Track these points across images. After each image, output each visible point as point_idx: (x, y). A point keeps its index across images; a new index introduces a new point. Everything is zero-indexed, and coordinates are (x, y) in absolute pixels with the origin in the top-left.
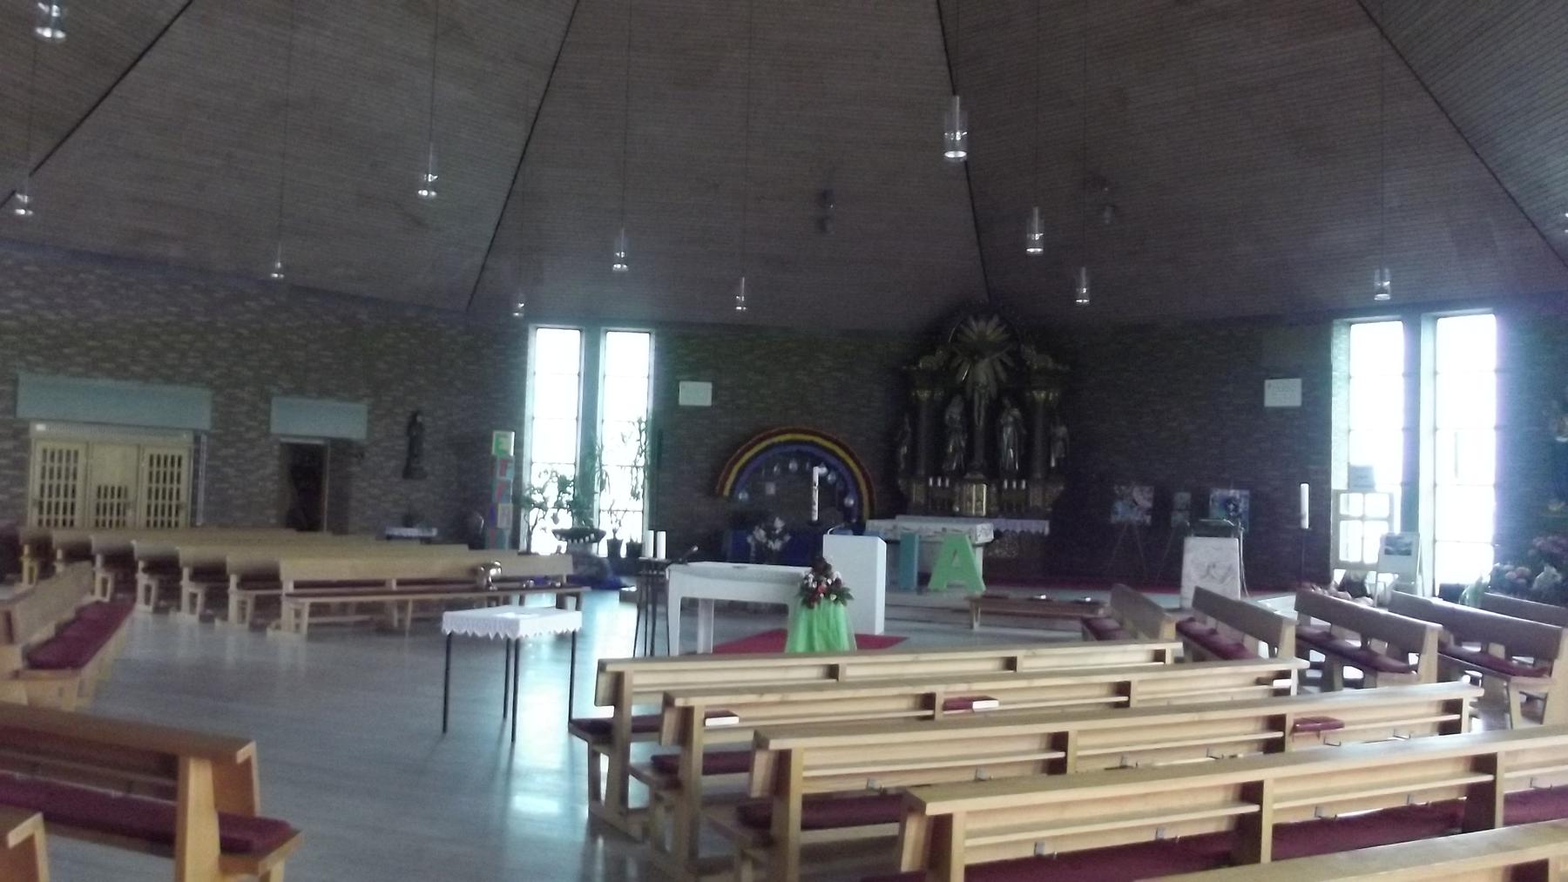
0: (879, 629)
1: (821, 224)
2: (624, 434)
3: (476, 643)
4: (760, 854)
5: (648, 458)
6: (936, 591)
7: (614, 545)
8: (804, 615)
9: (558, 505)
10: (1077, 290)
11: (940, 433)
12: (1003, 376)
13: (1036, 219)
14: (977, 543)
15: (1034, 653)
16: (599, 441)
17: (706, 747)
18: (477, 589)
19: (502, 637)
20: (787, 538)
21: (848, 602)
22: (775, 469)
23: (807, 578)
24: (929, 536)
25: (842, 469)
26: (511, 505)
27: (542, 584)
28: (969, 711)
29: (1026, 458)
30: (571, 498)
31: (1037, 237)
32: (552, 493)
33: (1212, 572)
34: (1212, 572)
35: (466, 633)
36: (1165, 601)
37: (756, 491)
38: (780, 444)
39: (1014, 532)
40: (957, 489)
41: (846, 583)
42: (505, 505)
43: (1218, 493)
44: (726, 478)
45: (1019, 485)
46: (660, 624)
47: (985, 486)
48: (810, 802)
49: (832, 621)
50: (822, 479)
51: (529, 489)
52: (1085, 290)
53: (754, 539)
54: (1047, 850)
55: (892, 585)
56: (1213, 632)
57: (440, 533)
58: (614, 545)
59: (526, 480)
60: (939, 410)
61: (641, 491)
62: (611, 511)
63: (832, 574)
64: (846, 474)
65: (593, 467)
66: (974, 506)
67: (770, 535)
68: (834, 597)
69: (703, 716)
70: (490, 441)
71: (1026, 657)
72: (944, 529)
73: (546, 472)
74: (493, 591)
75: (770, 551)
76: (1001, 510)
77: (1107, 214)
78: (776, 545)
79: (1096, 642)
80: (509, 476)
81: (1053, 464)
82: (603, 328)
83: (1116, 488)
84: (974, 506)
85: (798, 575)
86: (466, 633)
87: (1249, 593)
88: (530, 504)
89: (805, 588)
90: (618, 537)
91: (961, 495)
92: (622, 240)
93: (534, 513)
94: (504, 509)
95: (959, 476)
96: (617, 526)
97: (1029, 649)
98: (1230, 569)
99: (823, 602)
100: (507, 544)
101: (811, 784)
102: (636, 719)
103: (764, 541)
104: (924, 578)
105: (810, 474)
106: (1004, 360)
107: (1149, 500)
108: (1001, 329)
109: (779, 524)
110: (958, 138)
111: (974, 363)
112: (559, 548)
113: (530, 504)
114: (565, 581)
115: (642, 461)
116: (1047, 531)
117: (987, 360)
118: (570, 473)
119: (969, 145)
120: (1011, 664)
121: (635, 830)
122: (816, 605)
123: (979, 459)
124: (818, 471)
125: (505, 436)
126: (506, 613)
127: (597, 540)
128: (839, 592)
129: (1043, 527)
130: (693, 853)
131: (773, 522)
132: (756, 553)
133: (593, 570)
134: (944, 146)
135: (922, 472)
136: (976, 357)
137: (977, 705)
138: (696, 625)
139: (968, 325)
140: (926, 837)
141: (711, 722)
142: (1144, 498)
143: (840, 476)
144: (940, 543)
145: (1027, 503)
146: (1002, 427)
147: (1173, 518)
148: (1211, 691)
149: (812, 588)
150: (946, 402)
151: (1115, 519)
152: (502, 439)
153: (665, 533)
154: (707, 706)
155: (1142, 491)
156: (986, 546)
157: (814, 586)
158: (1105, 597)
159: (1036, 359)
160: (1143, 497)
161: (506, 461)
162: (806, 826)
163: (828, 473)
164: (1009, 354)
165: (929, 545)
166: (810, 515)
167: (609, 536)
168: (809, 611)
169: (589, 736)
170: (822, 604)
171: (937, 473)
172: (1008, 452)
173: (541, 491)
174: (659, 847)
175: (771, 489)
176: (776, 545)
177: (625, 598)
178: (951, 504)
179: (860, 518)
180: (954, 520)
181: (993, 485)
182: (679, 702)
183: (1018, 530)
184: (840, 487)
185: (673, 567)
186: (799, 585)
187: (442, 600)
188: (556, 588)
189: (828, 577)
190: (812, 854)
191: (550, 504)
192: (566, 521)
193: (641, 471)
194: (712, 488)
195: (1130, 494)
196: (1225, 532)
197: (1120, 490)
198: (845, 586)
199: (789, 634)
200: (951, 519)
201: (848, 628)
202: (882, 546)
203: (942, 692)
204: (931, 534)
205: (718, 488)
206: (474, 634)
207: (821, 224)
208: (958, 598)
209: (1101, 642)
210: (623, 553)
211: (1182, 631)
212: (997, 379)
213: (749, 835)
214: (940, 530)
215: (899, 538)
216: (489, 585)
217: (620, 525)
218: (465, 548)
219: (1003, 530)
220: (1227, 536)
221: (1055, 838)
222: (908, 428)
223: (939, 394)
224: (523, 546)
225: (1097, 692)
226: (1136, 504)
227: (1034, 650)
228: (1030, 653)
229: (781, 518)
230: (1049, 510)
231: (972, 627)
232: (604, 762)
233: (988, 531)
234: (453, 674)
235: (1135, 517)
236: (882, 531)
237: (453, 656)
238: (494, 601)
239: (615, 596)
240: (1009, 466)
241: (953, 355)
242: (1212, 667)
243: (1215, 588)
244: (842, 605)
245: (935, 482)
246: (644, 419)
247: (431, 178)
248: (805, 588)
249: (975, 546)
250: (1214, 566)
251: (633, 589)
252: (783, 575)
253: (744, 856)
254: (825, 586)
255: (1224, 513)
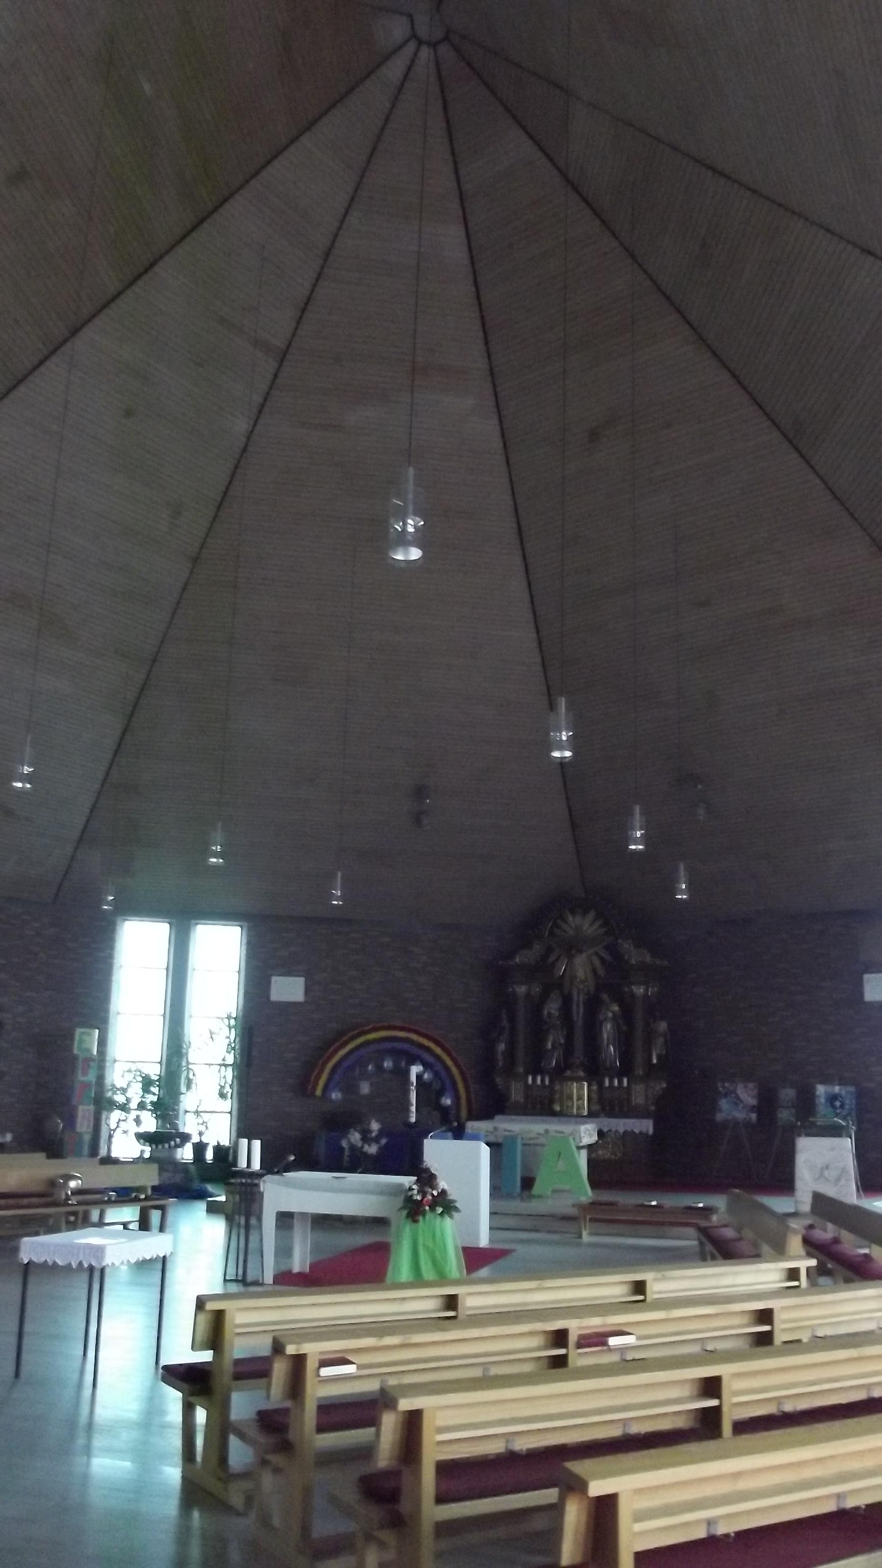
0: (484, 1241)
1: (418, 819)
2: (213, 1030)
3: (50, 1269)
4: (387, 1536)
5: (237, 1056)
6: (540, 1197)
7: (199, 1148)
8: (408, 1229)
9: (141, 1106)
10: (677, 886)
11: (538, 1029)
12: (601, 972)
13: (637, 816)
14: (581, 1144)
15: (663, 1275)
16: (186, 1039)
17: (319, 1399)
18: (55, 1204)
19: (86, 1265)
20: (384, 1141)
21: (455, 1214)
22: (370, 1067)
23: (411, 1189)
24: (530, 1139)
25: (439, 1067)
26: (92, 1108)
27: (125, 1195)
28: (605, 1348)
29: (626, 1055)
30: (155, 1099)
31: (638, 834)
32: (135, 1093)
33: (826, 1173)
34: (826, 1173)
35: (46, 1261)
36: (779, 1204)
37: (350, 1088)
38: (375, 1041)
39: (616, 1131)
40: (557, 1087)
41: (452, 1195)
42: (86, 1107)
43: (821, 1090)
44: (318, 1077)
45: (620, 1082)
46: (253, 1238)
47: (586, 1084)
48: (445, 1469)
49: (438, 1233)
50: (419, 1077)
51: (111, 1090)
52: (684, 886)
53: (349, 1142)
54: (721, 1529)
55: (496, 1191)
56: (836, 1241)
57: (15, 1139)
58: (199, 1148)
59: (108, 1081)
60: (536, 1006)
61: (230, 1091)
62: (197, 1113)
63: (437, 1184)
64: (443, 1074)
65: (179, 1066)
66: (575, 1105)
67: (366, 1137)
68: (439, 1210)
69: (317, 1365)
70: (72, 1038)
71: (655, 1280)
72: (547, 1131)
73: (129, 1071)
74: (72, 1205)
75: (365, 1154)
76: (603, 1109)
77: (701, 812)
78: (372, 1149)
79: (724, 1262)
80: (91, 1077)
81: (655, 1061)
82: (193, 922)
83: (719, 1084)
84: (575, 1105)
85: (400, 1185)
86: (46, 1261)
87: (865, 1196)
88: (112, 1105)
89: (409, 1200)
90: (205, 1140)
91: (562, 1093)
92: (219, 835)
93: (116, 1115)
94: (84, 1111)
95: (559, 1074)
96: (203, 1128)
97: (659, 1271)
98: (844, 1170)
99: (429, 1216)
100: (86, 1150)
101: (445, 1448)
102: (238, 1362)
103: (360, 1144)
104: (528, 1183)
105: (408, 1072)
106: (603, 955)
107: (753, 1097)
108: (598, 923)
109: (375, 1126)
110: (564, 738)
111: (571, 957)
112: (142, 1152)
113: (112, 1105)
114: (149, 1192)
115: (230, 1059)
116: (651, 1131)
117: (584, 955)
118: (154, 1071)
119: (573, 743)
120: (639, 1287)
121: (236, 1500)
122: (421, 1218)
123: (579, 1055)
124: (415, 1070)
125: (89, 1034)
126: (88, 1238)
127: (181, 1145)
128: (442, 1202)
129: (646, 1126)
130: (305, 1530)
131: (369, 1124)
132: (350, 1156)
133: (178, 1178)
134: (550, 746)
135: (521, 1070)
136: (574, 952)
137: (613, 1341)
138: (291, 1238)
139: (566, 922)
140: (588, 1523)
141: (325, 1372)
142: (749, 1096)
143: (436, 1074)
144: (543, 1145)
145: (629, 1100)
146: (601, 1023)
147: (779, 1115)
148: (857, 1317)
149: (417, 1200)
150: (544, 998)
151: (719, 1117)
152: (85, 1038)
153: (259, 1141)
154: (321, 1353)
155: (745, 1087)
156: (590, 1147)
157: (419, 1198)
158: (719, 1202)
159: (634, 955)
160: (747, 1095)
161: (88, 1060)
162: (441, 1499)
163: (424, 1072)
164: (607, 948)
165: (531, 1146)
166: (408, 1117)
167: (195, 1139)
168: (414, 1225)
169: (186, 1386)
170: (427, 1217)
171: (536, 1070)
172: (608, 1047)
173: (124, 1091)
174: (265, 1521)
175: (365, 1088)
176: (372, 1149)
177: (213, 1209)
178: (551, 1101)
179: (458, 1119)
180: (555, 1119)
181: (594, 1083)
182: (291, 1350)
183: (621, 1131)
184: (436, 1086)
185: (268, 1178)
186: (403, 1197)
187: (14, 1217)
188: (140, 1200)
189: (433, 1187)
190: (445, 1529)
191: (134, 1105)
192: (150, 1124)
193: (230, 1069)
194: (304, 1087)
195: (734, 1092)
196: (835, 1131)
197: (724, 1087)
198: (451, 1198)
199: (393, 1249)
200: (550, 1118)
201: (454, 1239)
202: (485, 1151)
203: (575, 1327)
204: (531, 1135)
205: (309, 1087)
206: (55, 1263)
207: (418, 819)
208: (564, 1206)
209: (728, 1261)
210: (209, 1155)
211: (811, 1246)
212: (594, 972)
213: (374, 1513)
214: (542, 1131)
215: (500, 1140)
216: (68, 1198)
217: (207, 1128)
218: (40, 1157)
219: (605, 1130)
220: (839, 1135)
221: (729, 1516)
222: (505, 1023)
223: (537, 989)
224: (103, 1152)
225: (737, 1321)
226: (741, 1101)
227: (663, 1273)
228: (659, 1275)
229: (377, 1121)
230: (653, 1108)
231: (580, 1237)
232: (201, 1415)
233: (592, 1132)
234: (29, 1306)
235: (740, 1115)
236: (483, 1133)
237: (31, 1287)
238: (79, 1221)
239: (200, 1207)
240: (610, 1062)
241: (549, 950)
242: (855, 1289)
243: (830, 1191)
244: (449, 1218)
245: (534, 1080)
246: (234, 1015)
247: (27, 770)
248: (409, 1200)
249: (579, 1148)
250: (827, 1167)
251: (223, 1198)
252: (378, 1184)
253: (369, 1537)
254: (430, 1197)
255: (830, 1109)
